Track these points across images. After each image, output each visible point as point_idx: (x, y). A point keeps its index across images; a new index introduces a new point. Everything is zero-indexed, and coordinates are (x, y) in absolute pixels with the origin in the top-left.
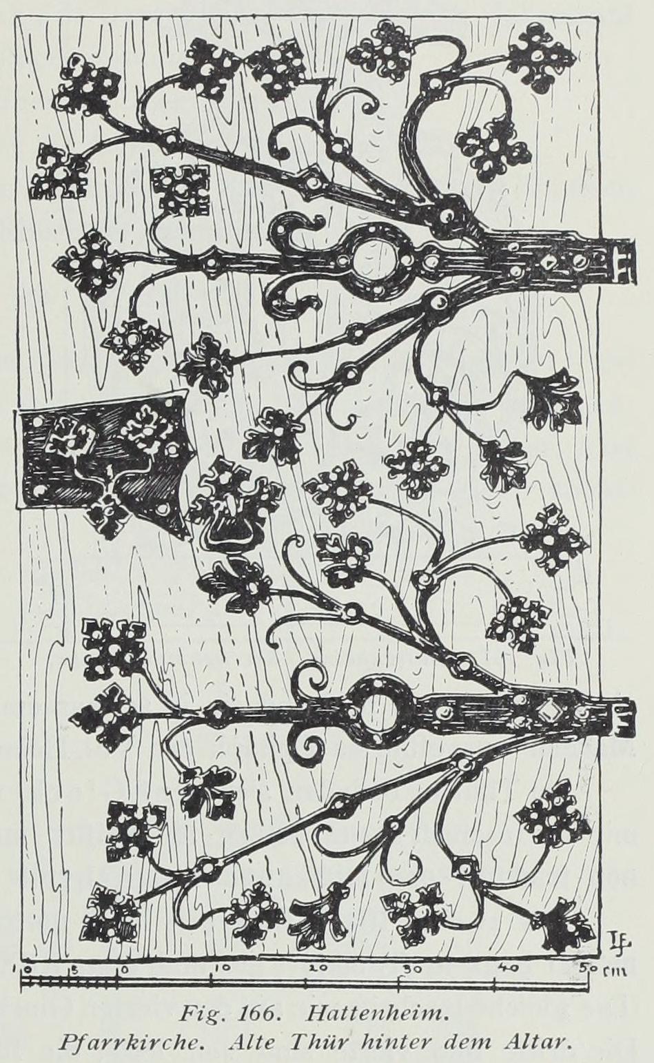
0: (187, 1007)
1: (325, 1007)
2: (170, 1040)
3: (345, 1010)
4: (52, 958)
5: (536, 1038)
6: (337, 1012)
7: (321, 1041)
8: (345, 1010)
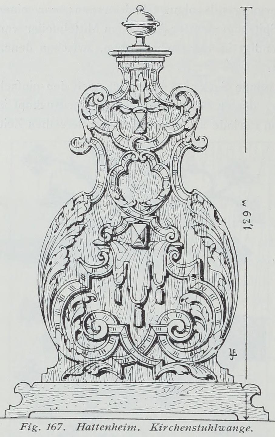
1: (84, 424)
2: (172, 426)
3: (94, 426)
5: (98, 426)
6: (90, 426)
8: (94, 426)
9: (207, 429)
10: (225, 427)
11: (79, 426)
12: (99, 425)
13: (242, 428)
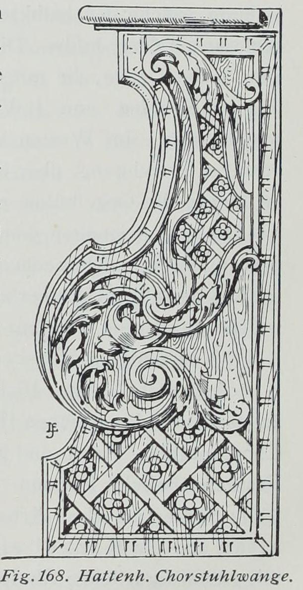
0: (6, 571)
1: (91, 571)
3: (106, 573)
4: (217, 540)
6: (100, 575)
7: (259, 576)
8: (106, 573)
9: (219, 577)
10: (248, 575)
11: (82, 575)
12: (115, 572)
13: (275, 576)
